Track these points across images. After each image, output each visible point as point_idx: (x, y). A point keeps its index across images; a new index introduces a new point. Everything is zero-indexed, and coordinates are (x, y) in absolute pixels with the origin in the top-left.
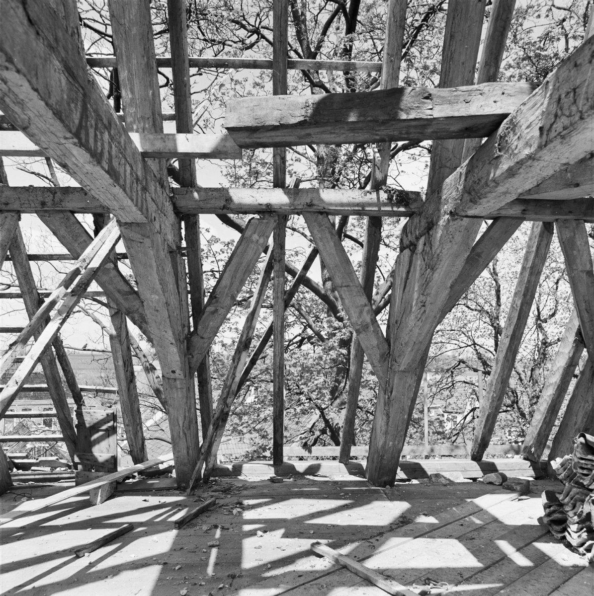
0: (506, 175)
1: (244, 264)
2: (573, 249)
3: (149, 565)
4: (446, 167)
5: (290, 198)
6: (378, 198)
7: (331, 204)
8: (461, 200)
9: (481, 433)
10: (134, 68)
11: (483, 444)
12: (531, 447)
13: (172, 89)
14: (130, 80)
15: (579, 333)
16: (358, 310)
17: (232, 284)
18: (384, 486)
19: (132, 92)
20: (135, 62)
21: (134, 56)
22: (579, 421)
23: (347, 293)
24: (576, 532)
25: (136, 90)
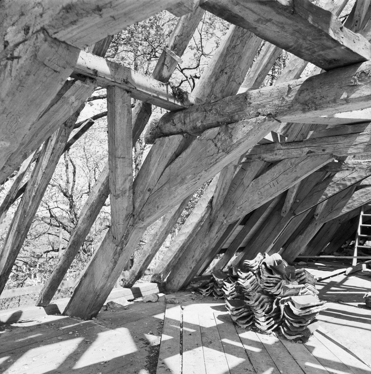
0: (364, 98)
1: (50, 124)
4: (235, 81)
5: (111, 70)
7: (139, 86)
12: (160, 274)
15: (211, 202)
16: (124, 178)
17: (30, 141)
18: (91, 319)
23: (122, 164)
24: (264, 322)
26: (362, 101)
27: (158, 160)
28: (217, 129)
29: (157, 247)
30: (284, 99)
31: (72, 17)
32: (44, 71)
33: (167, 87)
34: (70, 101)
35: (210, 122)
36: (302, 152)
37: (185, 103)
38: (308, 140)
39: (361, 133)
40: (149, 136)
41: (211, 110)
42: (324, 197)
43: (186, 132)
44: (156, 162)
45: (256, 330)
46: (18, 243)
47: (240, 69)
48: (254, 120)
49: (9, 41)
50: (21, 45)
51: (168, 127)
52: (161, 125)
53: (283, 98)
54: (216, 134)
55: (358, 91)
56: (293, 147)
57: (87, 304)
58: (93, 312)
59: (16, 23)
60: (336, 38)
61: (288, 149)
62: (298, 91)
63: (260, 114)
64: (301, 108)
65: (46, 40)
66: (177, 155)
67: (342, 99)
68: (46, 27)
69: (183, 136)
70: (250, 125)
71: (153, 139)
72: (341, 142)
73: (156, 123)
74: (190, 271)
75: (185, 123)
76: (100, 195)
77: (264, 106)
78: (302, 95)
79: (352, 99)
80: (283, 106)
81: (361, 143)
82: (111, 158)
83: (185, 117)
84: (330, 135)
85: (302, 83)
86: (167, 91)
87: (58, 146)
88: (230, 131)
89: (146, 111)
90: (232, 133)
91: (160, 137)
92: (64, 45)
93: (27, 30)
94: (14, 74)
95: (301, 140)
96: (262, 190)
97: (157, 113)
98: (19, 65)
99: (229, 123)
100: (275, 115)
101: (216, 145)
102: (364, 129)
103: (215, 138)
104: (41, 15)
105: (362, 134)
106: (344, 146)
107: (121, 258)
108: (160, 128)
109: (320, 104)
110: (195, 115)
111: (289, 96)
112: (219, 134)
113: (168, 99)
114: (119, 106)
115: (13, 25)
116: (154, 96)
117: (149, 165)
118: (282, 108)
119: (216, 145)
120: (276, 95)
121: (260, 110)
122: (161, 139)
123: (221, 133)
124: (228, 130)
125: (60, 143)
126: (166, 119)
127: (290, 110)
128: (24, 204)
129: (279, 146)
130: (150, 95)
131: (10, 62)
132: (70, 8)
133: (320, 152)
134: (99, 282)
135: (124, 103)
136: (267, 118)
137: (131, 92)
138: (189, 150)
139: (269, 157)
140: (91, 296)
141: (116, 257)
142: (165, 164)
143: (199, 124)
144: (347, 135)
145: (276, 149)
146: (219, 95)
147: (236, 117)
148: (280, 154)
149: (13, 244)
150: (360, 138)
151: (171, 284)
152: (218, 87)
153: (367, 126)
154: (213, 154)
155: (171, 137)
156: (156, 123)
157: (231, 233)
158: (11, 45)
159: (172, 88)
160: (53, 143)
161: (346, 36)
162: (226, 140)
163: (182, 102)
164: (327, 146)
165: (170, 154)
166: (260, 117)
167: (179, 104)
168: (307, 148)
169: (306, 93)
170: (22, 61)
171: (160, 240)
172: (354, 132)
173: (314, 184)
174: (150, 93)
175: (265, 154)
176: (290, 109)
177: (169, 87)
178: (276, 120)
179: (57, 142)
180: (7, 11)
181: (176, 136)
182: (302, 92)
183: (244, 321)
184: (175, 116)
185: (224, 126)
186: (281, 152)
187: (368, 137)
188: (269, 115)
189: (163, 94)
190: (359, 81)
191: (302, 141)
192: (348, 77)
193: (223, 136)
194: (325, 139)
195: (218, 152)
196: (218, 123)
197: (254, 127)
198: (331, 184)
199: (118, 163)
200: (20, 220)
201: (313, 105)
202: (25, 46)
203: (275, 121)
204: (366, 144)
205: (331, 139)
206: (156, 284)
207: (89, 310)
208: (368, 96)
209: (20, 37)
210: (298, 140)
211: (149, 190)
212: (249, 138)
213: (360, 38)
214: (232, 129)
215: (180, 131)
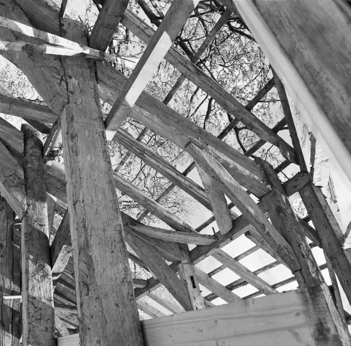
3: (293, 63)
8: (30, 225)
10: (156, 126)
13: (340, 238)
14: (151, 120)
19: (145, 116)
20: (158, 127)
21: (161, 129)
25: (146, 119)
26: (26, 267)
27: (6, 132)
28: (23, 177)
30: (36, 222)
31: (69, 119)
32: (52, 96)
33: (58, 148)
35: (29, 173)
36: (3, 241)
37: (46, 158)
38: (12, 244)
39: (12, 282)
40: (27, 128)
41: (38, 175)
43: (25, 155)
44: (5, 130)
47: (64, 196)
48: (25, 202)
49: (71, 80)
50: (66, 87)
51: (31, 143)
52: (34, 138)
53: (37, 221)
54: (19, 177)
55: (32, 264)
56: (8, 234)
59: (78, 86)
60: (63, 248)
61: (7, 230)
62: (40, 231)
63: (29, 206)
64: (28, 232)
65: (64, 102)
66: (8, 147)
67: (29, 256)
68: (69, 104)
69: (22, 153)
70: (22, 200)
71: (24, 131)
72: (7, 269)
73: (36, 134)
75: (32, 155)
77: (33, 209)
78: (37, 233)
79: (28, 261)
80: (31, 221)
81: (4, 282)
82: (11, 100)
83: (36, 156)
84: (14, 260)
85: (45, 233)
86: (56, 147)
88: (20, 186)
89: (45, 130)
90: (18, 188)
91: (24, 136)
92: (62, 109)
93: (72, 93)
94: (52, 79)
95: (14, 240)
97: (42, 137)
98: (56, 84)
99: (26, 186)
100: (26, 216)
101: (11, 176)
102: (15, 284)
103: (16, 176)
104: (76, 103)
105: (11, 282)
106: (3, 271)
108: (31, 137)
109: (28, 243)
110: (36, 163)
111: (38, 225)
112: (19, 179)
113: (50, 147)
115: (78, 84)
116: (52, 138)
118: (30, 220)
119: (11, 176)
120: (40, 217)
121: (31, 207)
122: (23, 137)
123: (19, 180)
124: (21, 185)
127: (28, 225)
129: (11, 223)
130: (53, 136)
131: (60, 77)
132: (72, 120)
135: (49, 118)
136: (25, 211)
137: (56, 124)
138: (10, 156)
143: (29, 165)
144: (12, 272)
145: (9, 221)
146: (47, 181)
147: (29, 191)
150: (8, 282)
152: (53, 181)
153: (18, 286)
154: (5, 173)
155: (23, 144)
156: (36, 134)
158: (69, 80)
159: (58, 151)
161: (65, 255)
162: (13, 183)
163: (47, 156)
164: (5, 258)
165: (9, 142)
166: (26, 206)
167: (46, 154)
168: (6, 244)
169: (38, 235)
170: (57, 86)
172: (14, 278)
174: (54, 136)
175: (5, 212)
176: (29, 225)
177: (58, 149)
178: (23, 217)
180: (87, 82)
181: (23, 148)
182: (39, 233)
184: (39, 149)
185: (24, 182)
186: (6, 225)
187: (8, 287)
188: (27, 212)
189: (53, 144)
190: (39, 265)
191: (12, 240)
192: (43, 259)
193: (17, 181)
194: (11, 257)
195: (5, 177)
196: (28, 179)
197: (20, 202)
201: (28, 239)
202: (64, 90)
203: (22, 216)
204: (3, 286)
205: (11, 261)
208: (28, 270)
209: (71, 87)
210: (14, 238)
212: (12, 199)
213: (65, 264)
214: (21, 188)
215: (26, 151)
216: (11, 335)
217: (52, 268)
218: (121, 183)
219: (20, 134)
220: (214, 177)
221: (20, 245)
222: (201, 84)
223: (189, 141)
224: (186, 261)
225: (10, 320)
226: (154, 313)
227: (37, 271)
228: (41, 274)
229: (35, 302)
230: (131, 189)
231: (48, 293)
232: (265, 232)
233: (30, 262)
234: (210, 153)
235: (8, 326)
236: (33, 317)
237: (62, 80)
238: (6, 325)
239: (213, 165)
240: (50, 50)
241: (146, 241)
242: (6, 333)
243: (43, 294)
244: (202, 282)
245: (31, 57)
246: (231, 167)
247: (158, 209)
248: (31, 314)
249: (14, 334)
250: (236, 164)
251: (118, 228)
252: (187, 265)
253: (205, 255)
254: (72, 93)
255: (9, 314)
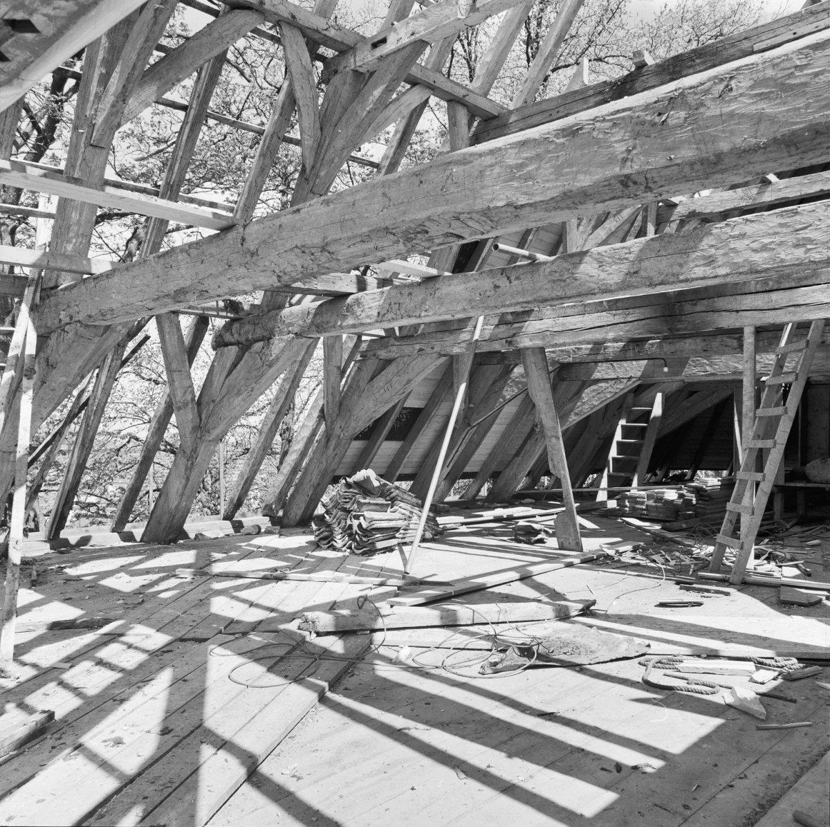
2: (332, 351)
6: (217, 305)
9: (237, 494)
11: (238, 504)
15: (322, 411)
16: (183, 391)
22: (314, 477)
29: (255, 468)
32: (82, 340)
34: (118, 329)
42: (502, 400)
43: (242, 344)
45: (334, 549)
46: (83, 457)
51: (228, 338)
57: (162, 527)
58: (171, 537)
66: (235, 365)
74: (308, 499)
76: (166, 407)
87: (114, 364)
95: (410, 334)
96: (377, 396)
107: (193, 474)
112: (263, 348)
114: (166, 326)
117: (212, 375)
125: (115, 361)
126: (227, 327)
128: (87, 417)
133: (428, 350)
134: (173, 502)
138: (242, 362)
139: (383, 354)
140: (167, 517)
141: (188, 472)
142: (225, 375)
143: (250, 337)
144: (451, 332)
148: (393, 352)
149: (79, 458)
151: (288, 517)
157: (374, 451)
158: (63, 323)
160: (109, 361)
165: (228, 365)
171: (258, 458)
173: (490, 382)
179: (112, 361)
183: (325, 542)
186: (395, 348)
188: (296, 334)
198: (509, 381)
199: (174, 376)
200: (84, 434)
205: (439, 335)
206: (268, 518)
207: (165, 534)
211: (213, 401)
216: (527, 323)
217: (348, 295)
218: (247, 199)
219: (219, 352)
220: (124, 100)
221: (419, 325)
222: (6, 148)
223: (90, 148)
224: (352, 60)
225: (509, 326)
226: (542, 61)
227: (353, 314)
228: (356, 306)
229: (382, 313)
230: (251, 183)
231: (375, 296)
232: (162, 7)
233: (344, 324)
234: (96, 111)
235: (515, 328)
236: (396, 314)
237: (63, 330)
238: (514, 332)
239: (110, 99)
240: (31, 349)
241: (327, 142)
242: (524, 330)
243: (376, 303)
244: (408, 5)
245: (54, 366)
246: (104, 71)
247: (272, 130)
248: (394, 316)
249: (527, 319)
250: (98, 63)
251: (156, 259)
252: (357, 59)
253: (326, 30)
254: (71, 318)
255: (503, 328)
